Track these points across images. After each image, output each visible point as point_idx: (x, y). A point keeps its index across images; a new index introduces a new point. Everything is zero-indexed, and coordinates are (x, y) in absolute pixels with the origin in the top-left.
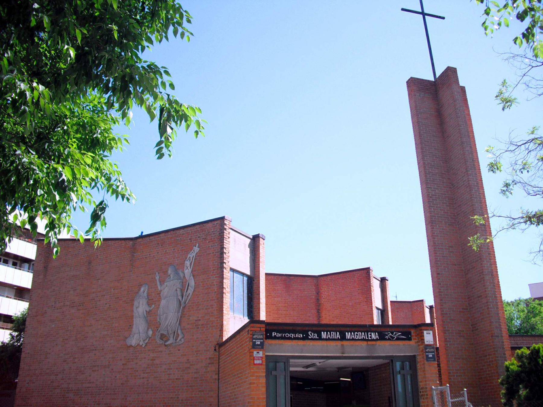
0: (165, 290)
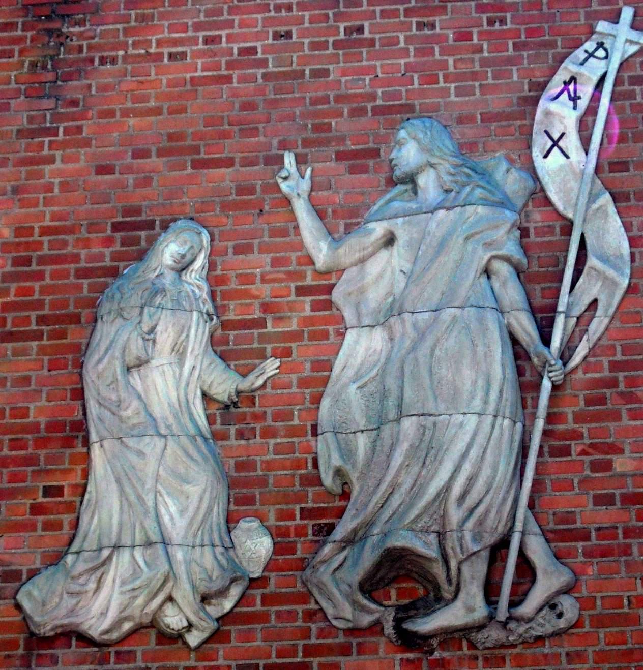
0: (374, 267)
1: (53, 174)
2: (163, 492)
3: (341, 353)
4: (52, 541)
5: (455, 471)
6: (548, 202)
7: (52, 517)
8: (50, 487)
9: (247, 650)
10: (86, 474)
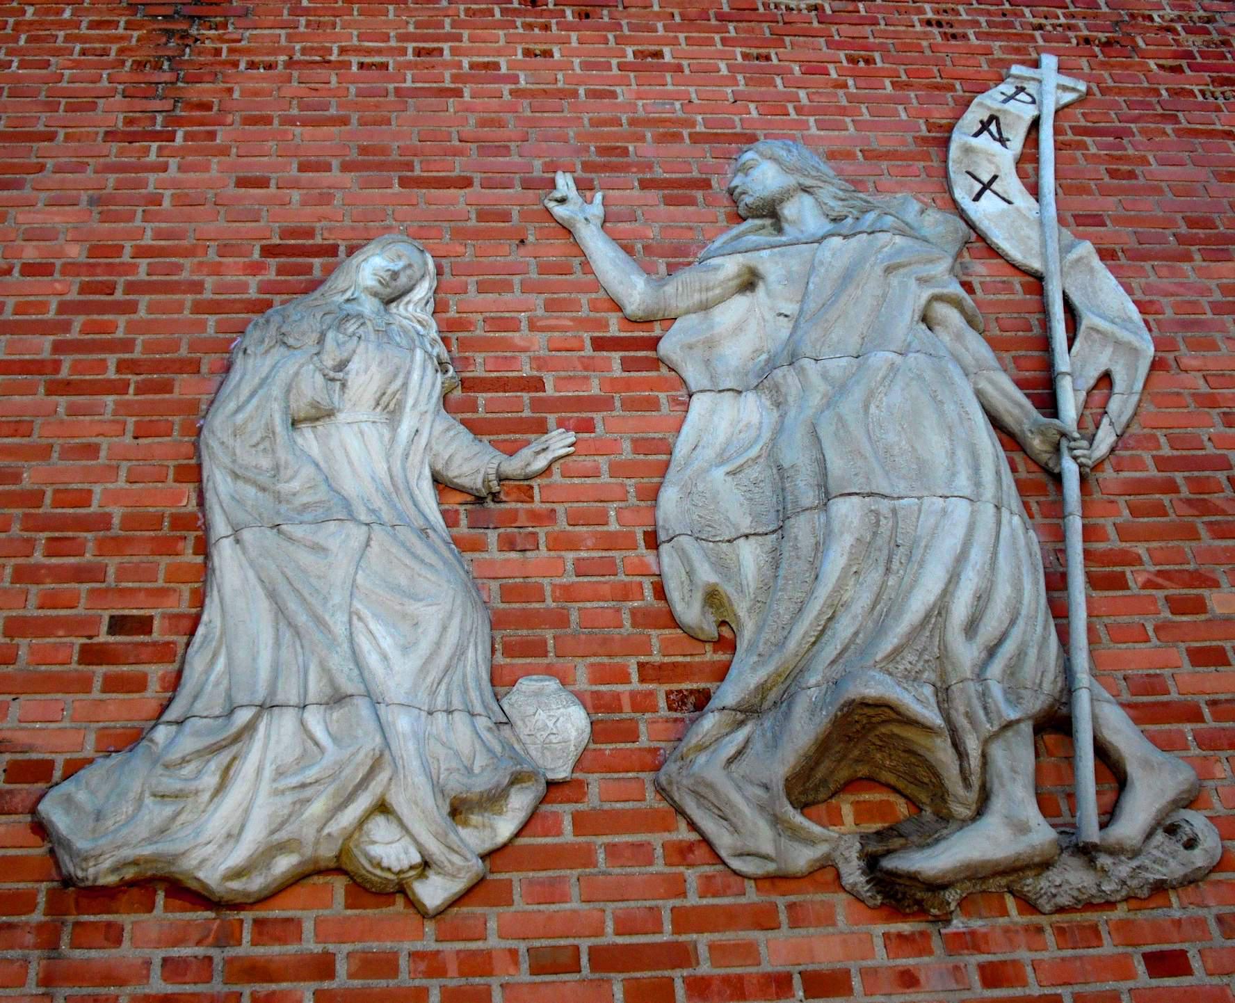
1: (162, 185)
2: (365, 613)
3: (686, 429)
4: (121, 710)
5: (949, 582)
6: (993, 252)
7: (125, 668)
8: (124, 617)
9: (550, 917)
10: (199, 599)
